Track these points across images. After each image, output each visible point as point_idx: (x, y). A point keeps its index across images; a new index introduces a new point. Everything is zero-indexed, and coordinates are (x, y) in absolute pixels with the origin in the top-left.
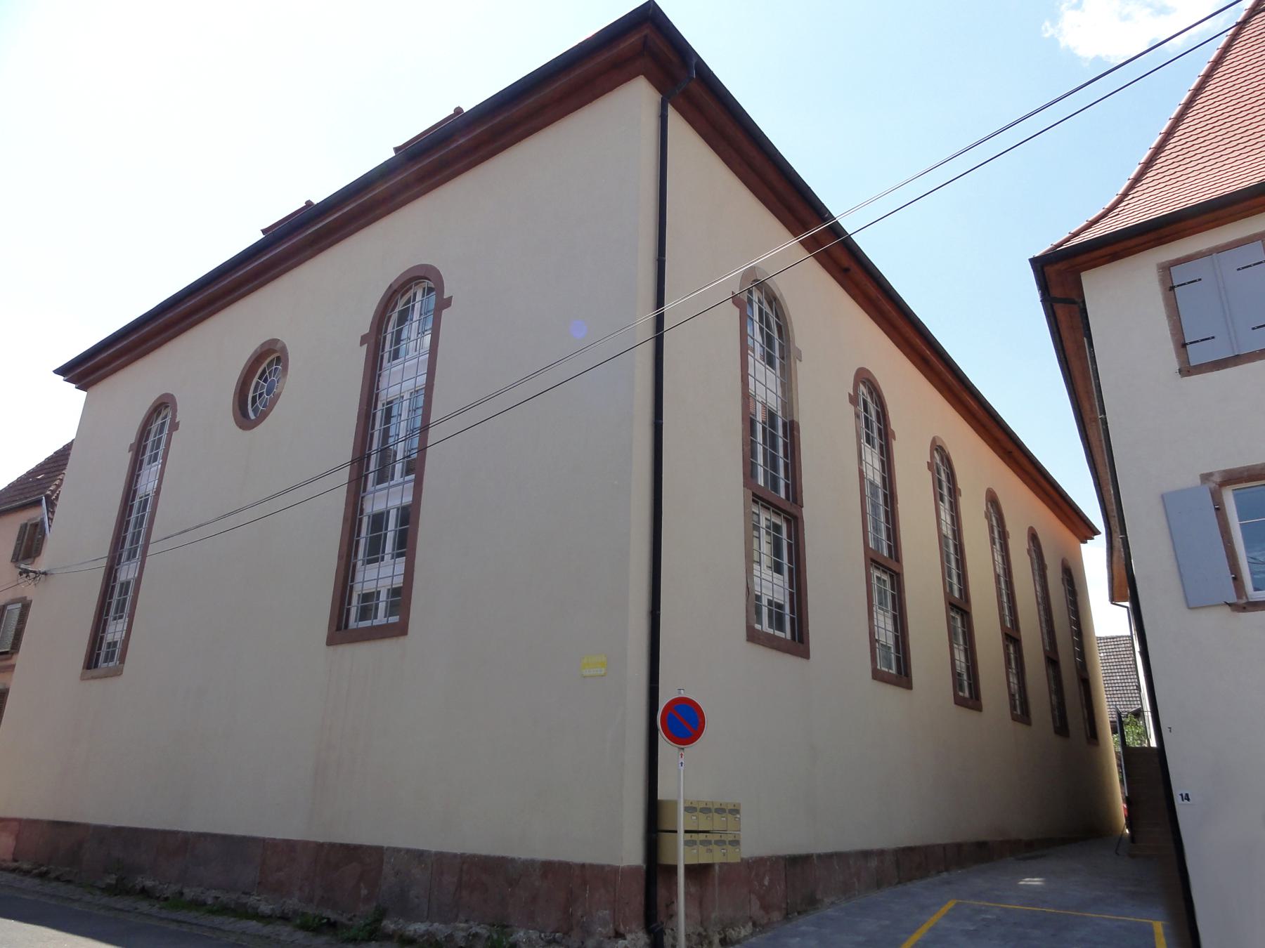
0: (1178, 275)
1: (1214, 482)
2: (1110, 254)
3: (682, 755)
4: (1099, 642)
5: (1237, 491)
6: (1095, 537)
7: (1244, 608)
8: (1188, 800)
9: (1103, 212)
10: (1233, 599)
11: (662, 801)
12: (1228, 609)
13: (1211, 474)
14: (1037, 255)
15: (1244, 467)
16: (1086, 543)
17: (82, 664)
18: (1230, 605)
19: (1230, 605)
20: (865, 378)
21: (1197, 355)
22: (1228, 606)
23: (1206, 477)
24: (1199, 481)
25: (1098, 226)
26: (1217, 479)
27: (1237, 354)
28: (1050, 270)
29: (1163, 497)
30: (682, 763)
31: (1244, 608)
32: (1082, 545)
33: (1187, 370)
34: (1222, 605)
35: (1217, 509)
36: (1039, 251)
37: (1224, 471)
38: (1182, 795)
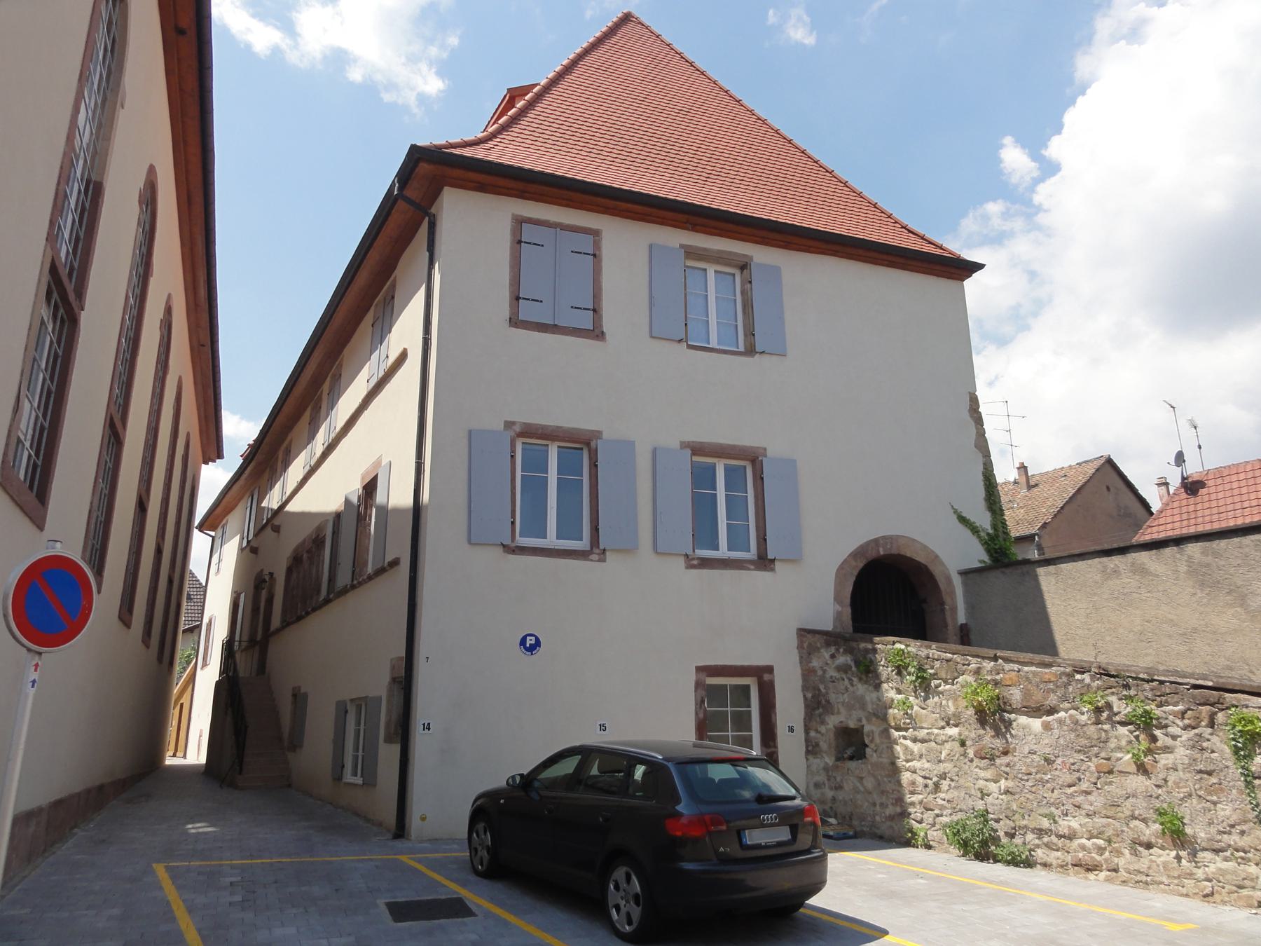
0: (528, 232)
1: (514, 431)
2: (479, 183)
3: (37, 665)
4: (191, 579)
5: (527, 446)
6: (218, 461)
7: (514, 551)
8: (429, 729)
9: (474, 140)
10: (508, 542)
11: (835, 627)
12: (501, 549)
13: (513, 423)
14: (418, 144)
15: (540, 425)
16: (215, 462)
17: (144, 180)
18: (504, 546)
19: (504, 546)
20: (152, 170)
21: (528, 312)
22: (502, 547)
23: (509, 425)
24: (502, 426)
25: (468, 149)
26: (517, 428)
27: (556, 323)
28: (424, 168)
29: (470, 432)
30: (34, 682)
31: (514, 551)
32: (203, 466)
33: (515, 322)
34: (499, 545)
35: (512, 456)
36: (423, 142)
37: (524, 423)
38: (424, 725)
